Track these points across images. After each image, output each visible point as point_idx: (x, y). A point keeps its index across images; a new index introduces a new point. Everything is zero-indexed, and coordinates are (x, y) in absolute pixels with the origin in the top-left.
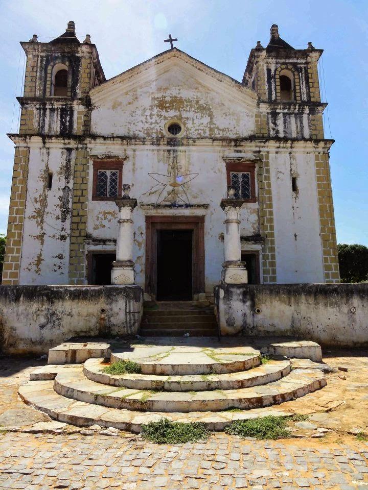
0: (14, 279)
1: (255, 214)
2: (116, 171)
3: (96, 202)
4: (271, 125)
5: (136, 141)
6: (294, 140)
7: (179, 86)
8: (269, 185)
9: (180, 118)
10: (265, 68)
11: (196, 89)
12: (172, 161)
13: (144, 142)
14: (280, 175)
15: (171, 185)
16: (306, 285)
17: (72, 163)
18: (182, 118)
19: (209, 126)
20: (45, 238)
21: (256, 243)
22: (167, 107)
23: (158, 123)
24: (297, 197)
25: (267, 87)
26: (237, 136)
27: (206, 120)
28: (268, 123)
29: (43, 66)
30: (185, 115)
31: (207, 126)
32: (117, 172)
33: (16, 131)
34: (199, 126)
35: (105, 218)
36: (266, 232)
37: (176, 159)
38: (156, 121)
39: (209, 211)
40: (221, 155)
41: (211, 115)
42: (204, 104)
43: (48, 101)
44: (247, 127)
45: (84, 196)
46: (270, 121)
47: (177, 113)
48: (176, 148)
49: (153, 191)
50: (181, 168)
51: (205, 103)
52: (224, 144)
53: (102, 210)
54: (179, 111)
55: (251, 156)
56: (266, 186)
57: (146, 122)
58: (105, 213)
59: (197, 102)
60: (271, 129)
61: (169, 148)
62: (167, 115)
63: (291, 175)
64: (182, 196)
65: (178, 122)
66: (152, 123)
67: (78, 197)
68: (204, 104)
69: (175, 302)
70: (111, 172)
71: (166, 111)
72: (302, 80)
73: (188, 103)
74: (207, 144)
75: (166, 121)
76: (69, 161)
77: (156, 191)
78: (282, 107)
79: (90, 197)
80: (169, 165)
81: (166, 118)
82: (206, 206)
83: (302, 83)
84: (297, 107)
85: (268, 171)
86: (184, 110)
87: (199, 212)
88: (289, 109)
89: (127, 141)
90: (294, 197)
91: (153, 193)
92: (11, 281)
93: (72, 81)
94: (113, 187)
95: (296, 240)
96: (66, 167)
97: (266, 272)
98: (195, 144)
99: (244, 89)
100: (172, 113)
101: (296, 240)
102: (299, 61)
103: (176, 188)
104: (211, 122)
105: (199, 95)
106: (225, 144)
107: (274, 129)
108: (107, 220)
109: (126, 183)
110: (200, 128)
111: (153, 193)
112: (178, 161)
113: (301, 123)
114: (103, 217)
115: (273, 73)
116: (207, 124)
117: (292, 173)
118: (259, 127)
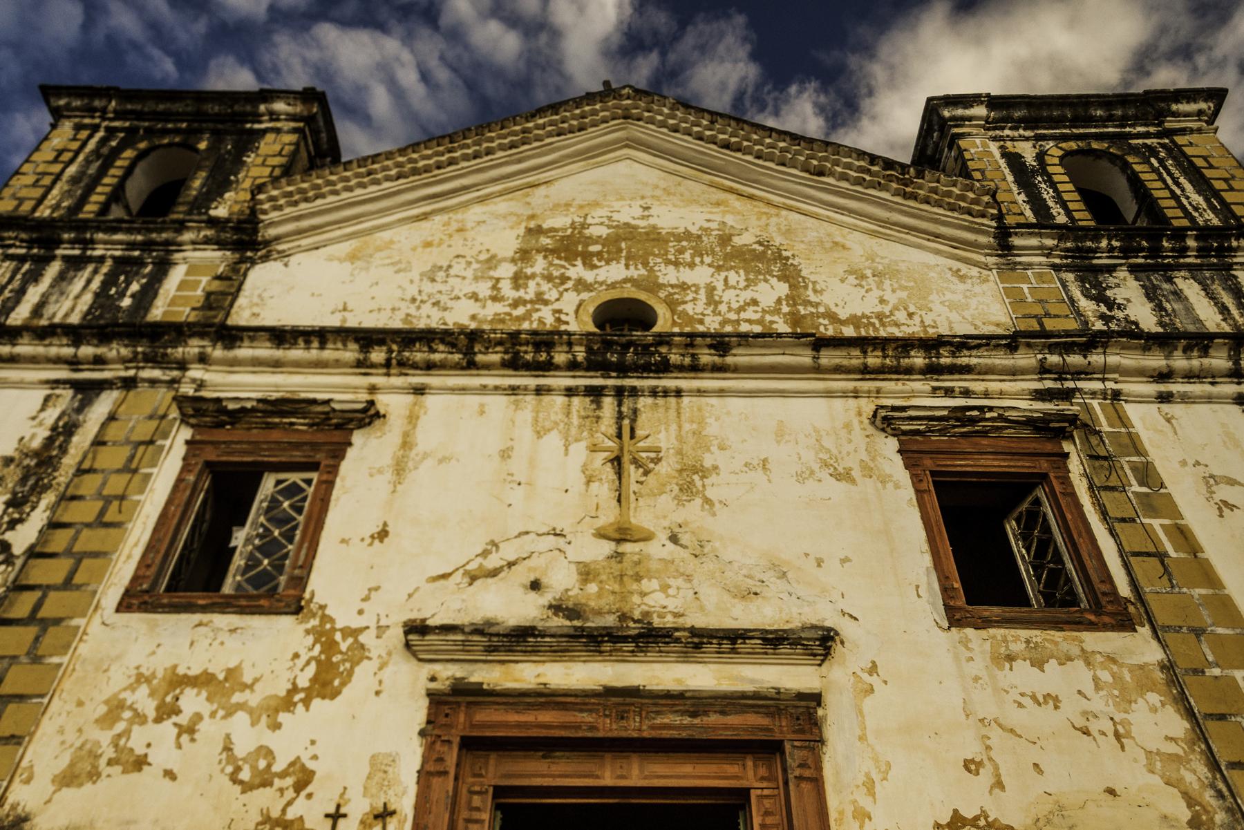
1: (1154, 698)
2: (285, 593)
5: (433, 351)
7: (643, 198)
8: (1182, 534)
9: (653, 286)
12: (612, 430)
13: (469, 352)
15: (601, 535)
17: (81, 441)
18: (661, 286)
19: (785, 309)
22: (592, 254)
23: (546, 303)
29: (105, 151)
31: (777, 311)
32: (309, 482)
34: (741, 309)
35: (167, 711)
37: (634, 421)
40: (868, 406)
41: (790, 275)
42: (756, 246)
45: (78, 587)
46: (1077, 293)
47: (637, 272)
49: (493, 562)
50: (657, 461)
51: (760, 243)
53: (159, 665)
54: (645, 264)
56: (1039, 132)
57: (495, 299)
58: (178, 681)
62: (589, 276)
64: (665, 588)
65: (642, 296)
66: (516, 303)
67: (38, 594)
68: (756, 246)
70: (279, 482)
71: (584, 264)
72: (1169, 173)
73: (684, 243)
75: (585, 295)
76: (64, 431)
77: (511, 565)
79: (111, 594)
80: (594, 449)
81: (581, 285)
83: (1178, 184)
86: (668, 262)
89: (390, 351)
91: (494, 573)
93: (203, 185)
96: (36, 454)
98: (729, 360)
99: (926, 184)
100: (614, 272)
103: (627, 548)
105: (730, 220)
106: (878, 361)
108: (167, 727)
109: (334, 616)
110: (743, 315)
111: (494, 573)
112: (640, 433)
114: (149, 707)
116: (779, 301)
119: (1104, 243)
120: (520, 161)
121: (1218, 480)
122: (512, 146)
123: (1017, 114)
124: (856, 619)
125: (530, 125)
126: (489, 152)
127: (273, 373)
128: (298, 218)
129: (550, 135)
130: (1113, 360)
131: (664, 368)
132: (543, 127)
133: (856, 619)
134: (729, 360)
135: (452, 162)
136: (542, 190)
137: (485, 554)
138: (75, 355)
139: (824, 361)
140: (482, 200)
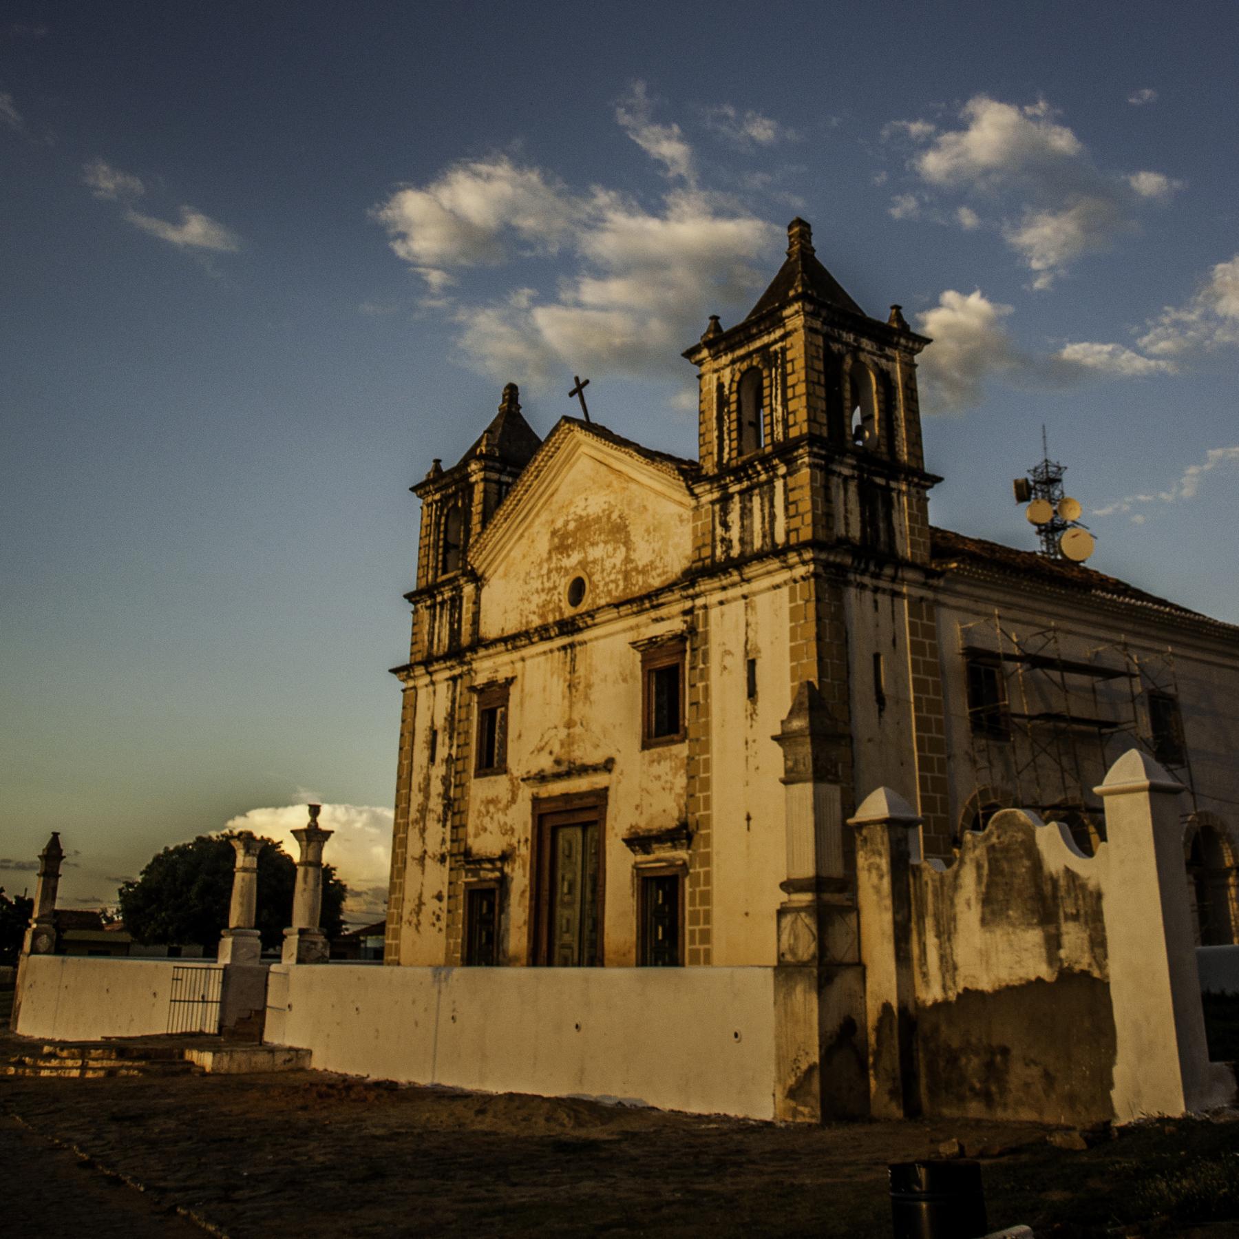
0: (939, 756)
3: (478, 780)
4: (719, 531)
10: (715, 383)
11: (609, 486)
20: (428, 861)
21: (674, 847)
24: (755, 710)
25: (716, 433)
26: (664, 578)
28: (714, 528)
30: (893, 484)
36: (697, 814)
38: (427, 608)
39: (614, 775)
41: (627, 543)
43: (444, 586)
44: (678, 556)
48: (578, 637)
52: (635, 609)
55: (677, 625)
59: (609, 517)
60: (718, 538)
63: (747, 653)
74: (610, 616)
78: (732, 478)
79: (472, 774)
82: (608, 765)
84: (759, 468)
85: (706, 655)
87: (600, 780)
88: (749, 478)
90: (749, 713)
92: (932, 758)
95: (748, 829)
101: (748, 829)
107: (723, 540)
113: (772, 506)
115: (727, 392)
117: (749, 647)
118: (704, 541)
119: (728, 480)
120: (544, 481)
121: (455, 872)
122: (537, 477)
123: (722, 347)
124: (1044, 426)
125: (536, 464)
126: (530, 486)
127: (572, 467)
128: (485, 560)
129: (548, 461)
130: (703, 588)
131: (580, 630)
132: (542, 460)
133: (1044, 426)
134: (596, 621)
135: (519, 500)
136: (555, 498)
137: (541, 741)
138: (499, 479)
139: (622, 613)
140: (537, 515)
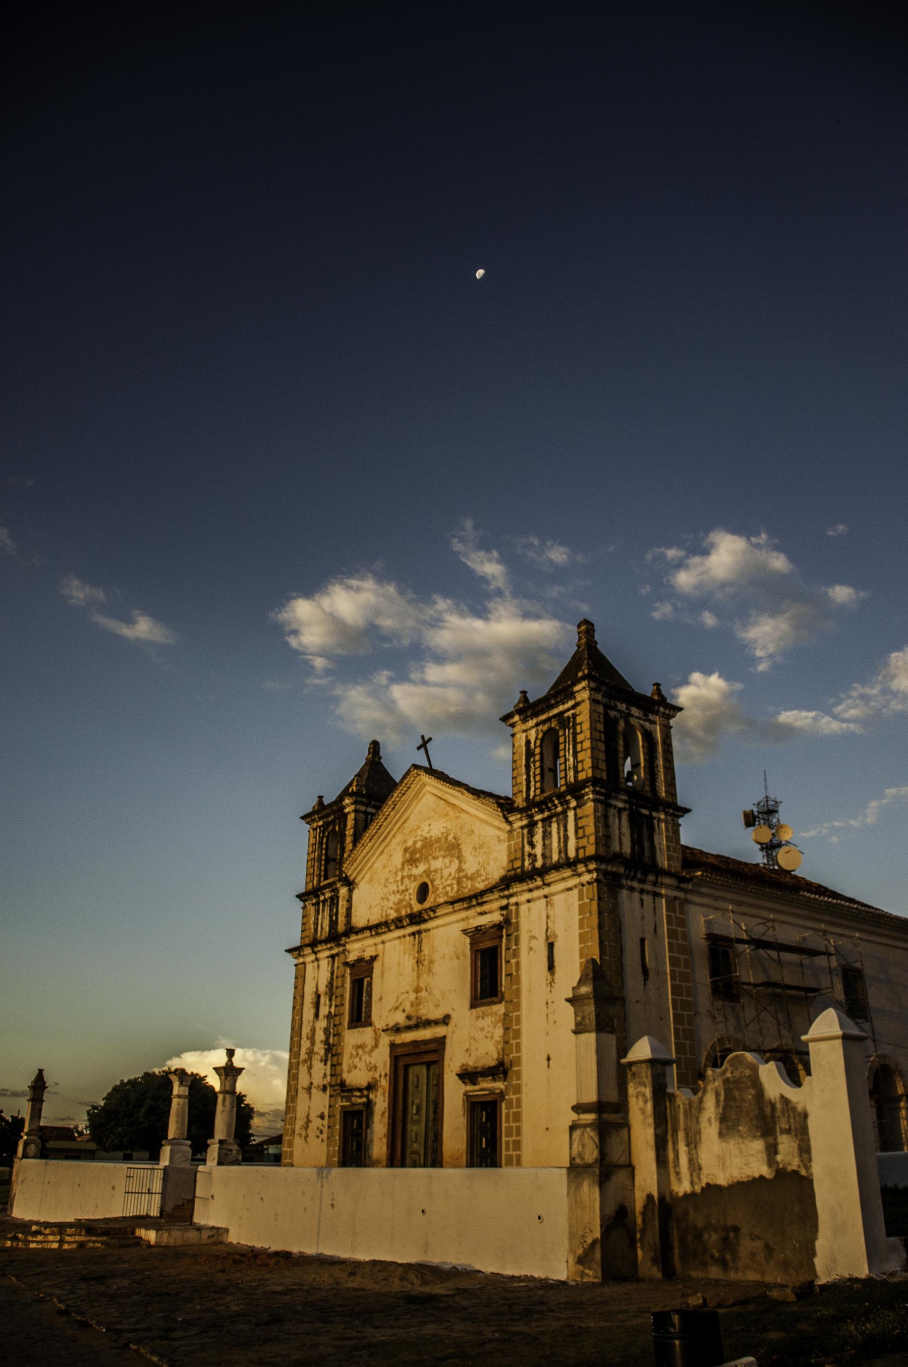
4: (527, 848)
6: (542, 872)
14: (533, 943)
16: (197, 1074)
21: (494, 1080)
24: (553, 979)
25: (524, 777)
26: (486, 883)
27: (456, 864)
28: (523, 846)
30: (654, 814)
33: (297, 942)
36: (511, 1056)
41: (460, 858)
48: (424, 926)
52: (465, 906)
55: (496, 917)
59: (446, 838)
61: (414, 929)
63: (547, 938)
69: (187, 1105)
74: (447, 911)
78: (537, 810)
79: (346, 1026)
82: (446, 1020)
88: (549, 809)
94: (687, 1006)
95: (549, 1067)
97: (509, 1134)
101: (549, 1067)
102: (561, 708)
104: (460, 870)
113: (566, 830)
115: (532, 746)
117: (549, 933)
